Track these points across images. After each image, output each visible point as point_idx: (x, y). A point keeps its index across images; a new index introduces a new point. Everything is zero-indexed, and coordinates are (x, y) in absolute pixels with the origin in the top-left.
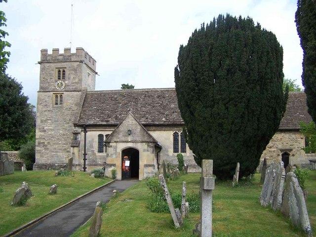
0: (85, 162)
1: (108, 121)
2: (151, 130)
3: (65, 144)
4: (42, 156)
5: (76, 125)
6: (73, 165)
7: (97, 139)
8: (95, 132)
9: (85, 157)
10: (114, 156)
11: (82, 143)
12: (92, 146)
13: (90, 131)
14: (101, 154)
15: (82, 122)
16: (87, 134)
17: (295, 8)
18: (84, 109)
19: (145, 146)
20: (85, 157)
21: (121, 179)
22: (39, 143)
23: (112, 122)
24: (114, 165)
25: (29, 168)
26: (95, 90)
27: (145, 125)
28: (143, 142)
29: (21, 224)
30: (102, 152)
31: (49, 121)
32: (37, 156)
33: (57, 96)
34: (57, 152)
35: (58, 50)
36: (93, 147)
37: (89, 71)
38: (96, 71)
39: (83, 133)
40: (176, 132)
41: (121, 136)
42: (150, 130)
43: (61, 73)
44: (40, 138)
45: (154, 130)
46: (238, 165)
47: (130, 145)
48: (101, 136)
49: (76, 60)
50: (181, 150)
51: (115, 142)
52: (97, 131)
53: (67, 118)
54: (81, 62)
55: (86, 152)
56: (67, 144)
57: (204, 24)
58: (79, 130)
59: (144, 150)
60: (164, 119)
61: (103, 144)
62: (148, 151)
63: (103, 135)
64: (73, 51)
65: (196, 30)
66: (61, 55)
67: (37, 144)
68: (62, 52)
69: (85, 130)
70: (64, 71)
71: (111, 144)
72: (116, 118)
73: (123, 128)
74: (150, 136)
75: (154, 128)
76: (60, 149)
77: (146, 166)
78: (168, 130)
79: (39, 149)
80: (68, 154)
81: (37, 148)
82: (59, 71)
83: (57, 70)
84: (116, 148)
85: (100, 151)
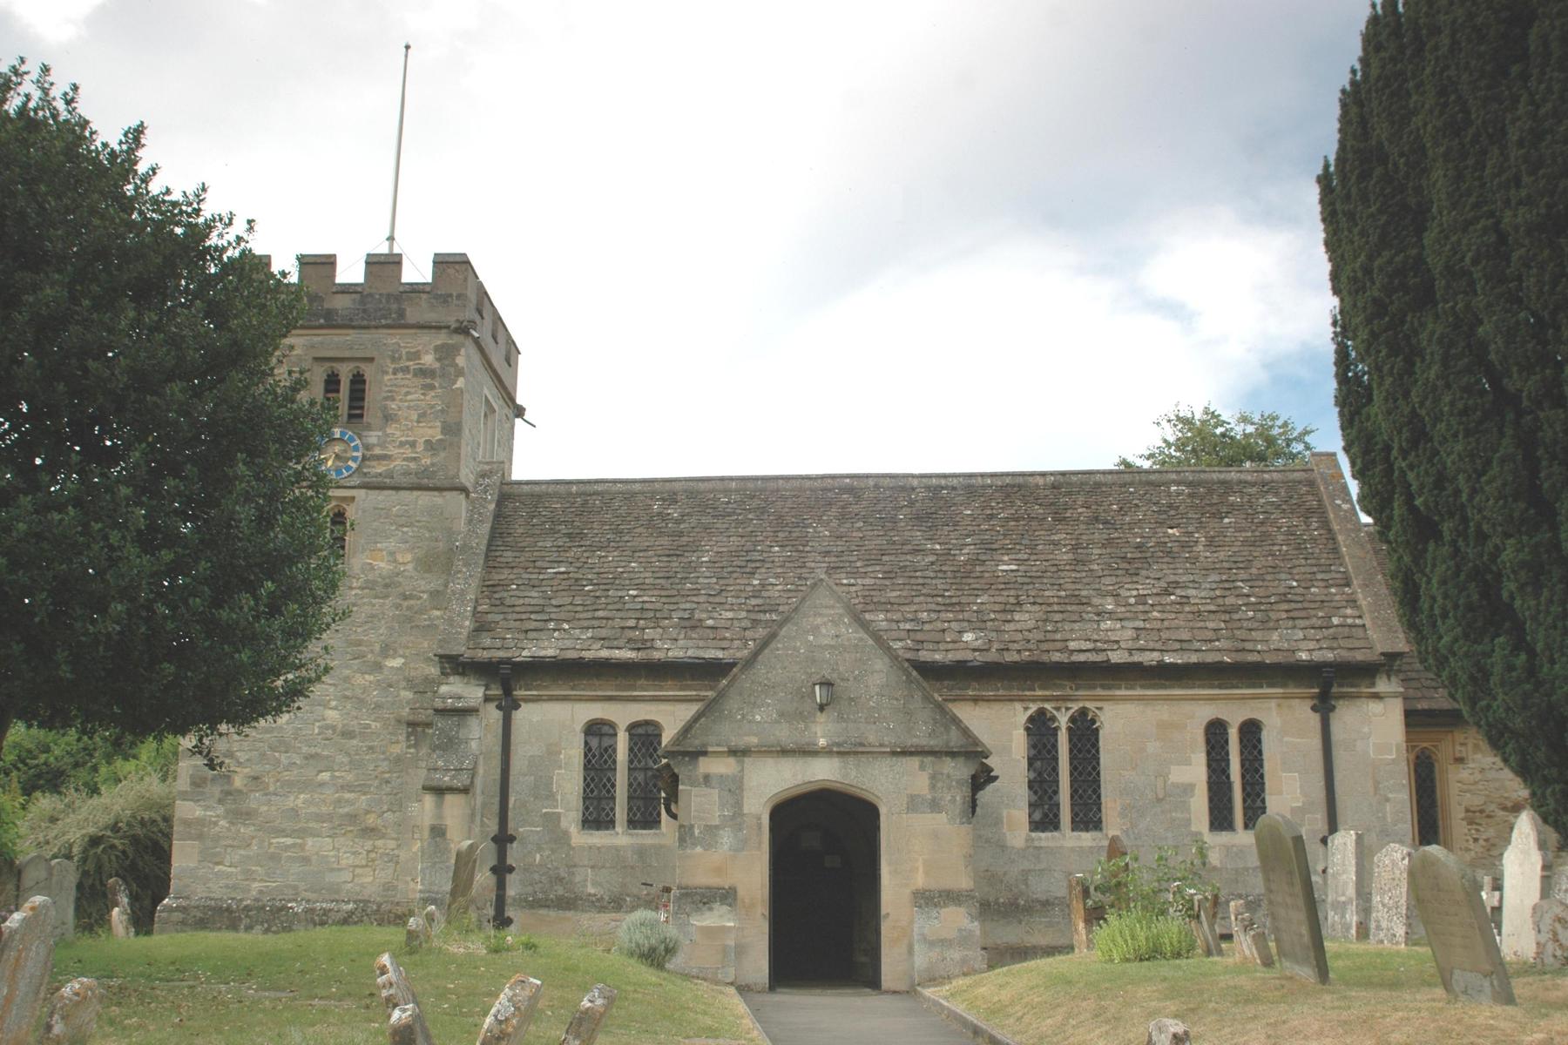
0: (501, 886)
1: (644, 645)
3: (348, 787)
6: (1324, 706)
7: (574, 753)
9: (502, 855)
10: (726, 839)
11: (487, 774)
12: (544, 791)
14: (598, 838)
16: (519, 716)
17: (1323, 235)
18: (496, 577)
19: (914, 777)
20: (502, 855)
21: (766, 979)
24: (727, 896)
25: (143, 921)
28: (905, 753)
30: (610, 824)
32: (183, 858)
34: (303, 833)
35: (328, 262)
36: (551, 796)
39: (493, 714)
40: (1042, 712)
46: (539, 982)
47: (823, 772)
48: (597, 730)
49: (430, 317)
50: (1075, 815)
51: (733, 752)
52: (580, 699)
53: (372, 636)
54: (463, 330)
55: (511, 825)
56: (362, 789)
58: (470, 692)
59: (914, 804)
60: (968, 637)
62: (935, 806)
63: (612, 725)
64: (418, 271)
66: (347, 289)
68: (351, 272)
69: (508, 692)
70: (358, 381)
71: (706, 766)
76: (320, 818)
77: (927, 899)
78: (997, 700)
79: (199, 813)
80: (368, 844)
84: (734, 789)
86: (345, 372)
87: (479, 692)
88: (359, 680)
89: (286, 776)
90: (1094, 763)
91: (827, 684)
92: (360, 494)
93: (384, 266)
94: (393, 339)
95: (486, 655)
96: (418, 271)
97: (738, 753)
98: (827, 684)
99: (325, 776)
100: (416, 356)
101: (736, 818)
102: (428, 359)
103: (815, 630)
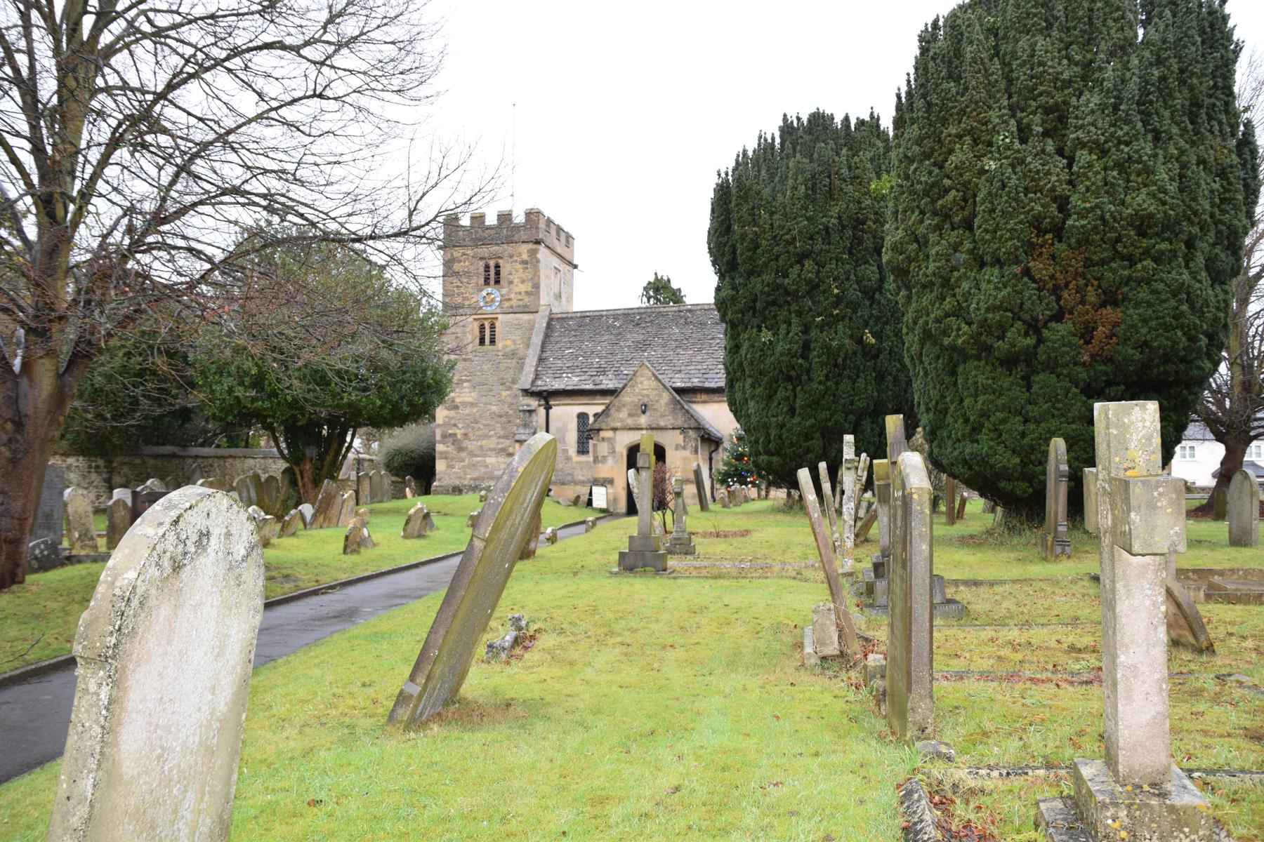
2: (698, 402)
4: (450, 467)
5: (527, 393)
8: (570, 407)
10: (610, 462)
13: (559, 405)
14: (583, 458)
15: (542, 385)
16: (552, 412)
19: (678, 437)
22: (444, 436)
23: (608, 383)
26: (575, 310)
27: (679, 391)
29: (954, 507)
31: (465, 384)
32: (440, 466)
33: (483, 325)
34: (485, 456)
37: (556, 262)
38: (575, 262)
39: (542, 411)
41: (621, 416)
42: (694, 402)
43: (492, 277)
44: (444, 425)
45: (704, 402)
48: (582, 417)
53: (508, 375)
54: (538, 242)
57: (899, 89)
58: (534, 403)
59: (677, 448)
61: (587, 433)
62: (684, 448)
64: (519, 218)
65: (745, 152)
66: (490, 228)
67: (438, 437)
69: (547, 403)
70: (497, 266)
71: (602, 434)
72: (618, 373)
73: (628, 398)
74: (690, 416)
75: (704, 397)
76: (491, 450)
81: (440, 448)
82: (487, 267)
83: (482, 263)
84: (611, 441)
85: (582, 450)
86: (492, 263)
87: (537, 403)
88: (505, 393)
89: (477, 433)
90: (161, 441)
91: (646, 406)
92: (500, 316)
93: (505, 218)
94: (509, 249)
95: (539, 388)
96: (519, 218)
97: (615, 429)
98: (646, 406)
99: (492, 433)
100: (520, 254)
101: (613, 452)
102: (525, 257)
103: (641, 383)
